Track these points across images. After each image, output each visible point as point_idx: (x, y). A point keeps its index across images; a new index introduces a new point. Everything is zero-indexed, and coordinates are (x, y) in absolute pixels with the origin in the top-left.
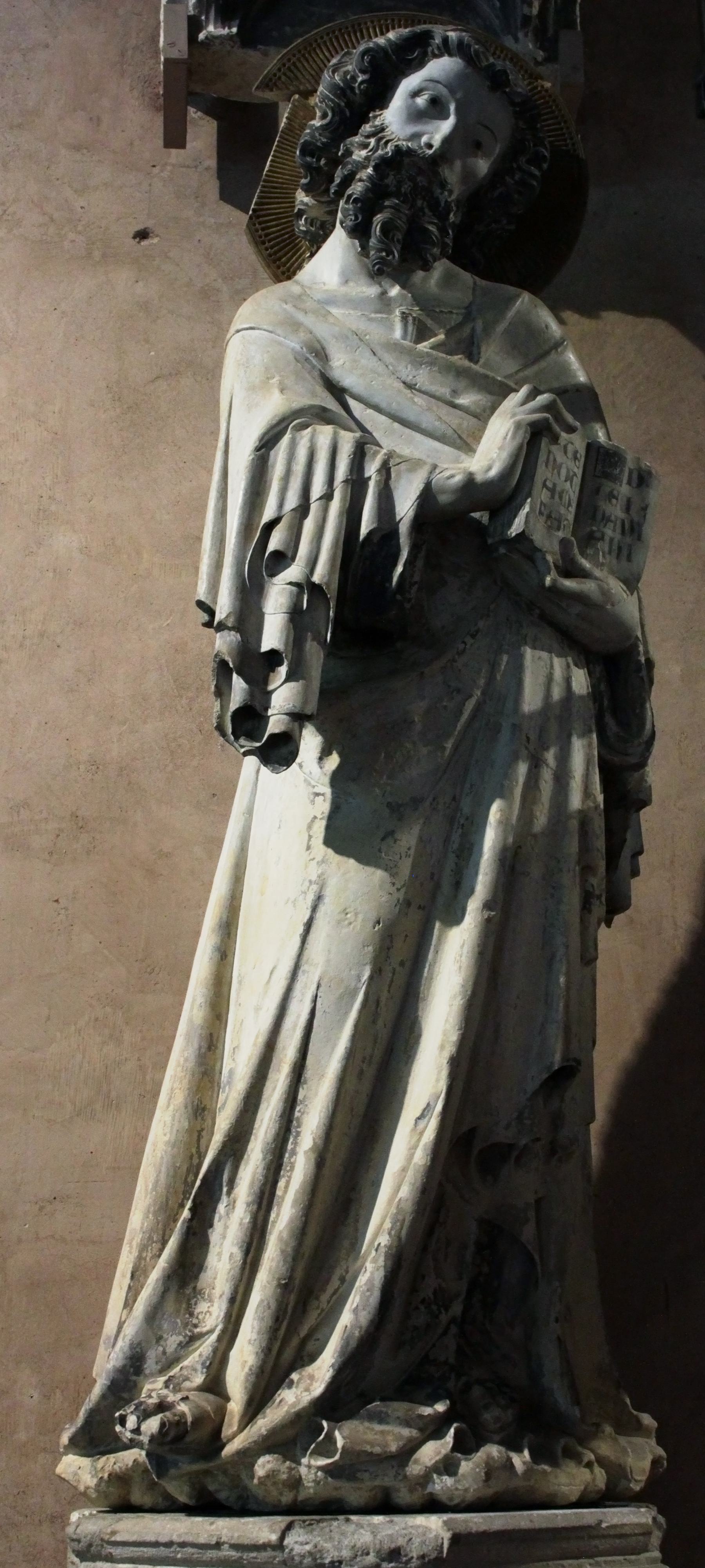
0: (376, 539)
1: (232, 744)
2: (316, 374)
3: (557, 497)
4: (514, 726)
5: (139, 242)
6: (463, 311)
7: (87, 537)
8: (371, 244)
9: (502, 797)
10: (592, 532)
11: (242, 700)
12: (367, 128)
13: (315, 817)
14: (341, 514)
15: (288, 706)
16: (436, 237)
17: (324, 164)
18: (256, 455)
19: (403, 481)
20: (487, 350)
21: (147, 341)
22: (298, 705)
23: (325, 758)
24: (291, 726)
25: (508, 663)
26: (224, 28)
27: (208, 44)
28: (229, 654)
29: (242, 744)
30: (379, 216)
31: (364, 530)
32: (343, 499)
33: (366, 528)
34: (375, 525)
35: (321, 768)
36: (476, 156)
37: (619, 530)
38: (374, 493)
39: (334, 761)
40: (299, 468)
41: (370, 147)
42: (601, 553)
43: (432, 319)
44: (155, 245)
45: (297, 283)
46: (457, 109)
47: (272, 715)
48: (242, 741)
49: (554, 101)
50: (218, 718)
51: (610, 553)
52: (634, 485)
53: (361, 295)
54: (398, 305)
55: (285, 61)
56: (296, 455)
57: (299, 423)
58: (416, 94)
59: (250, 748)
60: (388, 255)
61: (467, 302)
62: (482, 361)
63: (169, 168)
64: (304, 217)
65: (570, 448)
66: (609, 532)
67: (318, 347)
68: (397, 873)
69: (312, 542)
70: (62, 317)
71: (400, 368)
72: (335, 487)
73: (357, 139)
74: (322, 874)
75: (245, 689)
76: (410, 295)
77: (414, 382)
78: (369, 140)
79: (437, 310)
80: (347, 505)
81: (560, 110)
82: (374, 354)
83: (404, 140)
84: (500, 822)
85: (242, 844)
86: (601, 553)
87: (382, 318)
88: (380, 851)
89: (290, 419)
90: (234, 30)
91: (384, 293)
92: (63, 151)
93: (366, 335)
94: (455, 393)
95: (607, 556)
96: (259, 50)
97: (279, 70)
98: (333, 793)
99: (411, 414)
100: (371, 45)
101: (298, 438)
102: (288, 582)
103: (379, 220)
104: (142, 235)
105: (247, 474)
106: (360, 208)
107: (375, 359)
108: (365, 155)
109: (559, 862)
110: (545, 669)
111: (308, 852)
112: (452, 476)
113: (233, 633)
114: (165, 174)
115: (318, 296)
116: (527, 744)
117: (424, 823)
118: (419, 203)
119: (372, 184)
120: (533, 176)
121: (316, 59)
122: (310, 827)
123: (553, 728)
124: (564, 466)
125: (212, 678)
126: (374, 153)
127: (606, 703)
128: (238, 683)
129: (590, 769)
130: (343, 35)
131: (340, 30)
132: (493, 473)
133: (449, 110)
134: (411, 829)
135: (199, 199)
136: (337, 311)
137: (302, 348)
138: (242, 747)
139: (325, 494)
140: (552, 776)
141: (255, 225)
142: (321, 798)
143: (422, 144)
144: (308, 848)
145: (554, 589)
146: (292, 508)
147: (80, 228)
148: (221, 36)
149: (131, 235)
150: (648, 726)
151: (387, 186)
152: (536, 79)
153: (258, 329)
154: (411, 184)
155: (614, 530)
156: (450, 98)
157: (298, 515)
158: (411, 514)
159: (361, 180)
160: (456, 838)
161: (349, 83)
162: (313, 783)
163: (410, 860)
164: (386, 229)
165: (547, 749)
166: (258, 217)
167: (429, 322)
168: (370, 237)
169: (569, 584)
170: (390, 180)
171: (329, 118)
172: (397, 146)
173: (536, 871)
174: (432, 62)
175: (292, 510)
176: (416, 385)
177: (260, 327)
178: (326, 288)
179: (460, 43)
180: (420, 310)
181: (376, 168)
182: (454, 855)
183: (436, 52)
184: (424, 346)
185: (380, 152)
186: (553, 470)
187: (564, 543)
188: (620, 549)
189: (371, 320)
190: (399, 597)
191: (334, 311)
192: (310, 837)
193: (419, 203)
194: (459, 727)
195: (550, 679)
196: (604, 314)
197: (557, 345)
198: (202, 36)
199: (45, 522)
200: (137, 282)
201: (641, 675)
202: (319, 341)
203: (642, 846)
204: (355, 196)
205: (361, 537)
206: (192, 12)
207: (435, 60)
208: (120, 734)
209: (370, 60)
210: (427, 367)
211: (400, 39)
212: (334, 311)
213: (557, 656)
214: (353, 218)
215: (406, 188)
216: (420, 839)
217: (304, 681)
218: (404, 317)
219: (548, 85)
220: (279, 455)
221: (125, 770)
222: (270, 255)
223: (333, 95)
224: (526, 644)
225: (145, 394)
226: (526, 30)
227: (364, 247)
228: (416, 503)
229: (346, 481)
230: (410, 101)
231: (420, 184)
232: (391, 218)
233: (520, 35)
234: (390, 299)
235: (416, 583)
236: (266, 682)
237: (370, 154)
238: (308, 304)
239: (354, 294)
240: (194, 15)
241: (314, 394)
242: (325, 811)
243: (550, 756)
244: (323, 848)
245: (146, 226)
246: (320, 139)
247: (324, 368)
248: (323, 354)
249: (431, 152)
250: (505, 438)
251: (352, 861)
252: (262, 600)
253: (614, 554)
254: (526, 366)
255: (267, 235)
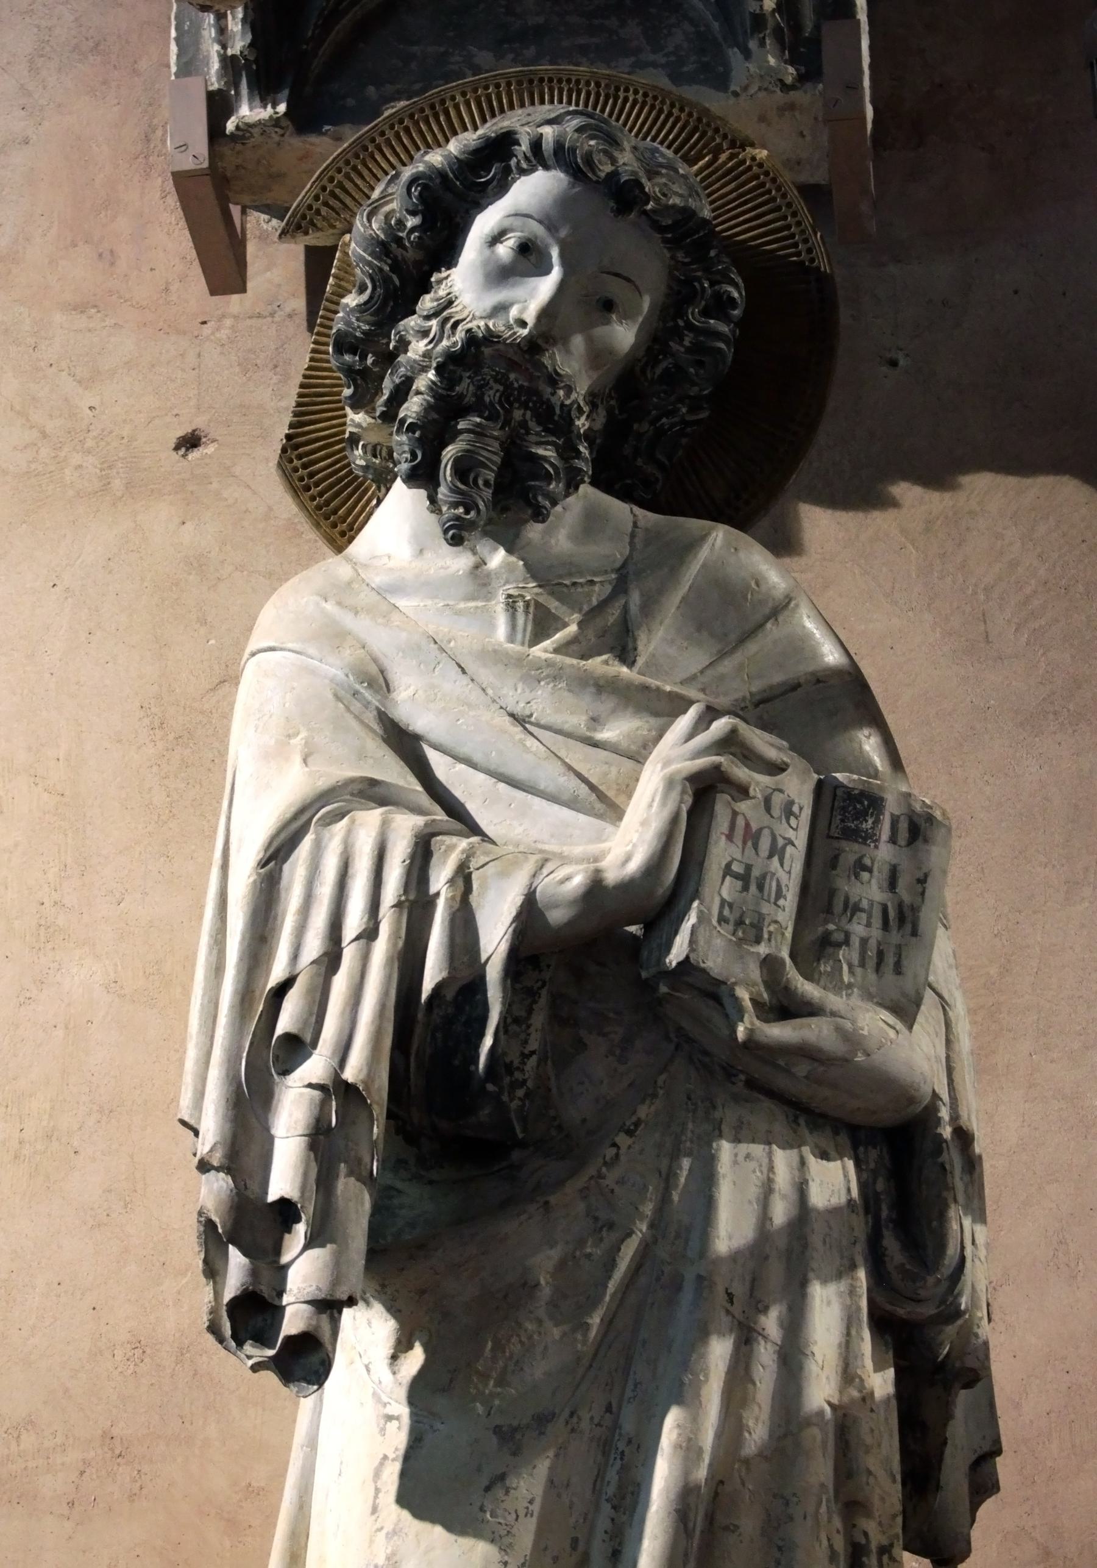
0: (450, 994)
1: (234, 1354)
2: (370, 717)
3: (753, 888)
4: (700, 1278)
5: (184, 456)
6: (614, 576)
7: (116, 965)
8: (440, 496)
9: (679, 1400)
10: (827, 935)
11: (239, 1285)
12: (427, 303)
13: (385, 1457)
14: (389, 962)
15: (309, 1290)
16: (552, 464)
17: (373, 364)
18: (259, 874)
19: (491, 895)
20: (649, 641)
21: (203, 622)
22: (325, 1285)
23: (402, 1356)
24: (314, 1322)
25: (690, 1170)
26: (265, 107)
27: (243, 137)
28: (216, 1211)
29: (248, 1353)
30: (450, 448)
31: (428, 985)
32: (394, 935)
33: (432, 978)
34: (444, 974)
35: (394, 1373)
36: (608, 322)
37: (877, 922)
38: (443, 922)
39: (416, 1358)
40: (325, 890)
41: (431, 335)
42: (845, 968)
43: (559, 599)
44: (210, 457)
45: (349, 560)
46: (562, 256)
47: (288, 1304)
48: (249, 1348)
49: (774, 180)
50: (211, 1313)
51: (862, 964)
52: (903, 843)
53: (442, 573)
54: (502, 582)
55: (325, 182)
56: (322, 868)
57: (328, 813)
58: (496, 239)
59: (261, 1359)
60: (467, 512)
61: (619, 559)
62: (640, 661)
63: (228, 322)
64: (361, 443)
65: (777, 800)
66: (858, 929)
67: (373, 670)
68: (511, 1545)
69: (343, 1013)
70: (66, 598)
71: (505, 691)
72: (381, 915)
73: (412, 322)
74: (394, 1554)
75: (244, 1265)
76: (521, 563)
77: (528, 713)
78: (430, 323)
79: (567, 582)
80: (401, 943)
81: (784, 196)
82: (464, 671)
83: (481, 318)
84: (677, 1446)
85: (301, 1497)
86: (845, 968)
87: (477, 607)
88: (482, 1509)
89: (318, 805)
90: (282, 108)
91: (481, 563)
92: (58, 318)
93: (449, 642)
94: (595, 721)
95: (859, 971)
96: (325, 134)
97: (317, 198)
98: (413, 1415)
99: (519, 771)
100: (421, 168)
101: (325, 840)
102: (306, 1083)
103: (449, 456)
104: (190, 442)
105: (245, 908)
106: (419, 440)
107: (465, 680)
108: (424, 349)
109: (787, 1504)
110: (758, 1174)
111: (374, 1517)
112: (568, 878)
113: (222, 1175)
114: (223, 334)
115: (377, 580)
116: (728, 1306)
117: (557, 1455)
118: (518, 414)
119: (433, 397)
120: (718, 335)
121: (398, 150)
122: (377, 1474)
123: (775, 1272)
124: (766, 832)
125: (197, 1249)
126: (436, 345)
127: (885, 1213)
128: (236, 1258)
129: (853, 1332)
130: (417, 124)
131: (412, 116)
132: (634, 866)
133: (551, 257)
134: (534, 1467)
135: (278, 369)
136: (409, 603)
137: (347, 676)
138: (249, 1357)
139: (364, 930)
140: (775, 1357)
141: (291, 461)
142: (395, 1423)
143: (512, 322)
144: (375, 1510)
145: (752, 1045)
146: (311, 959)
147: (90, 443)
148: (259, 122)
149: (172, 444)
150: (952, 1250)
151: (461, 396)
152: (743, 147)
153: (281, 649)
154: (501, 388)
155: (868, 925)
156: (550, 240)
157: (323, 969)
158: (504, 947)
159: (418, 393)
160: (612, 1475)
161: (394, 229)
162: (385, 1399)
163: (534, 1520)
164: (464, 469)
165: (765, 1310)
166: (296, 447)
167: (553, 605)
168: (438, 485)
169: (779, 1032)
170: (465, 387)
171: (369, 291)
172: (469, 331)
173: (749, 1524)
174: (518, 182)
175: (313, 962)
176: (531, 715)
177: (284, 646)
178: (391, 564)
179: (559, 147)
180: (540, 586)
181: (439, 370)
182: (609, 1506)
183: (524, 165)
184: (542, 651)
185: (445, 343)
186: (744, 843)
187: (770, 964)
188: (880, 954)
189: (459, 613)
190: (490, 1087)
191: (403, 603)
192: (377, 1491)
193: (518, 414)
194: (612, 1286)
195: (768, 1189)
196: (965, 480)
197: (779, 609)
198: (230, 126)
199: (49, 946)
200: (184, 523)
201: (940, 1160)
202: (375, 660)
203: (997, 1441)
204: (409, 421)
205: (424, 996)
206: (215, 85)
207: (523, 178)
208: (179, 1293)
209: (420, 193)
210: (548, 684)
211: (464, 153)
212: (403, 603)
213: (783, 1148)
214: (408, 456)
215: (491, 395)
216: (551, 1482)
217: (334, 1246)
218: (511, 603)
219: (762, 154)
220: (296, 869)
221: (188, 1351)
222: (319, 508)
223: (369, 255)
224: (720, 1136)
225: (202, 712)
226: (761, 35)
227: (432, 499)
228: (511, 930)
229: (398, 905)
230: (487, 252)
231: (516, 385)
232: (468, 451)
233: (753, 44)
234: (488, 575)
235: (533, 1053)
236: (278, 1251)
237: (430, 347)
238: (362, 595)
239: (432, 571)
240: (220, 91)
241: (362, 756)
242: (399, 1447)
243: (771, 1323)
244: (395, 1509)
245: (194, 428)
246: (359, 327)
247: (384, 706)
248: (381, 680)
249: (525, 332)
250: (650, 806)
251: (438, 1530)
252: (270, 1116)
253: (871, 963)
254: (722, 655)
255: (311, 475)
